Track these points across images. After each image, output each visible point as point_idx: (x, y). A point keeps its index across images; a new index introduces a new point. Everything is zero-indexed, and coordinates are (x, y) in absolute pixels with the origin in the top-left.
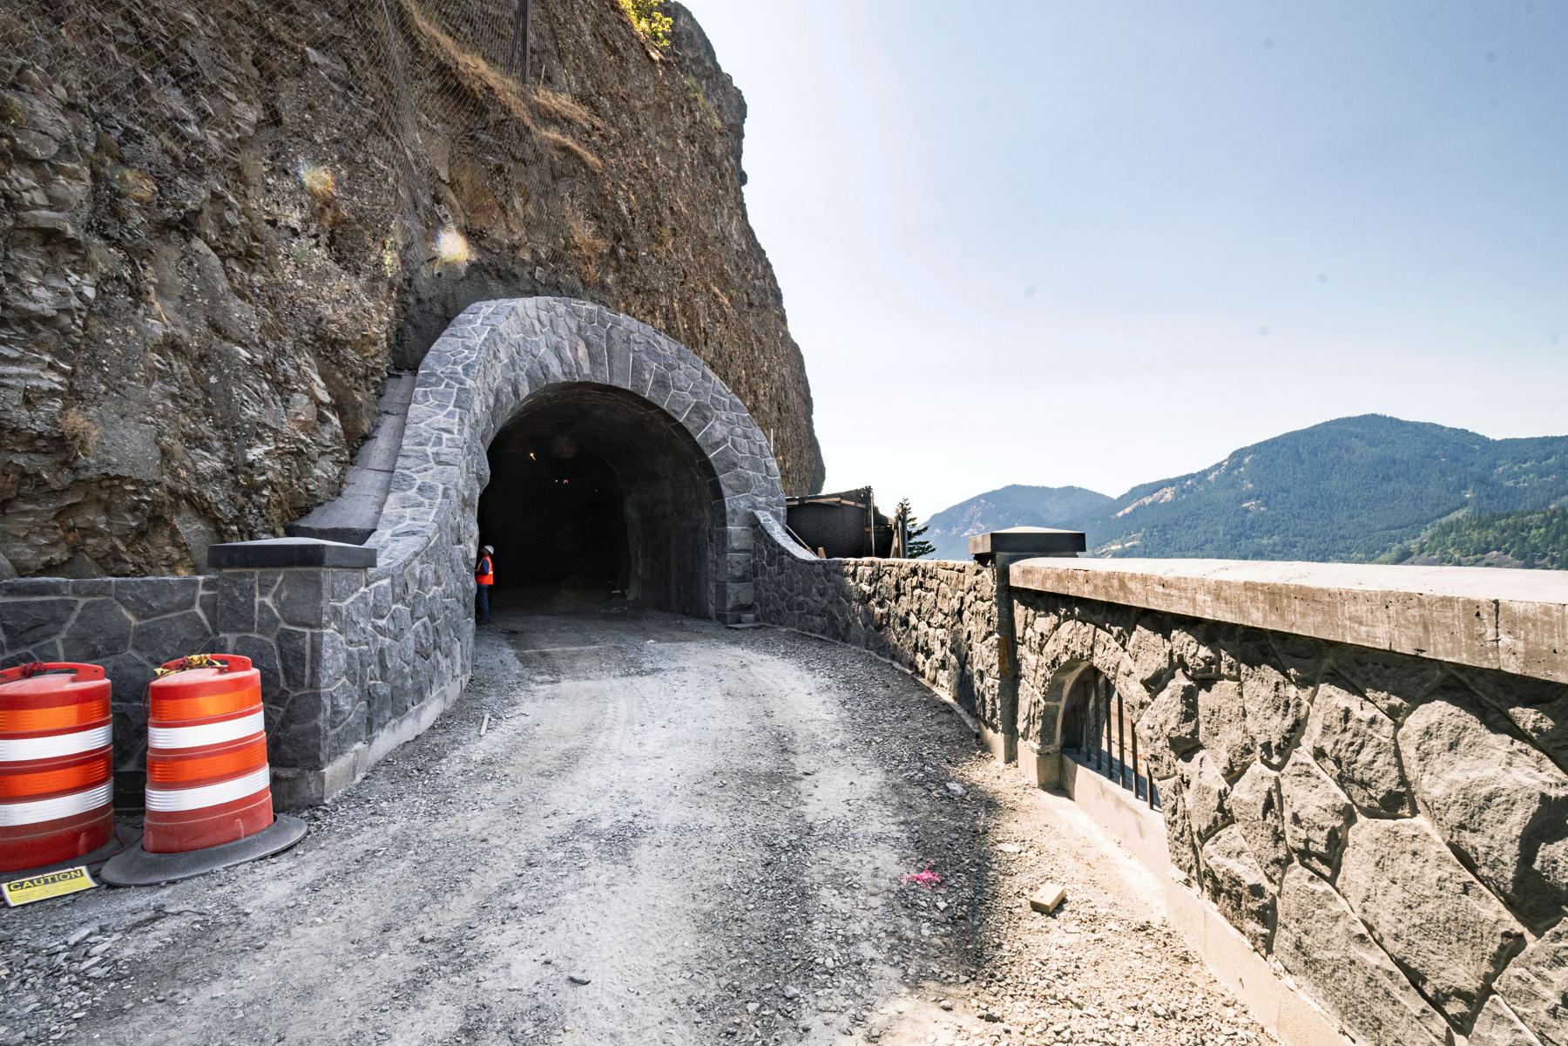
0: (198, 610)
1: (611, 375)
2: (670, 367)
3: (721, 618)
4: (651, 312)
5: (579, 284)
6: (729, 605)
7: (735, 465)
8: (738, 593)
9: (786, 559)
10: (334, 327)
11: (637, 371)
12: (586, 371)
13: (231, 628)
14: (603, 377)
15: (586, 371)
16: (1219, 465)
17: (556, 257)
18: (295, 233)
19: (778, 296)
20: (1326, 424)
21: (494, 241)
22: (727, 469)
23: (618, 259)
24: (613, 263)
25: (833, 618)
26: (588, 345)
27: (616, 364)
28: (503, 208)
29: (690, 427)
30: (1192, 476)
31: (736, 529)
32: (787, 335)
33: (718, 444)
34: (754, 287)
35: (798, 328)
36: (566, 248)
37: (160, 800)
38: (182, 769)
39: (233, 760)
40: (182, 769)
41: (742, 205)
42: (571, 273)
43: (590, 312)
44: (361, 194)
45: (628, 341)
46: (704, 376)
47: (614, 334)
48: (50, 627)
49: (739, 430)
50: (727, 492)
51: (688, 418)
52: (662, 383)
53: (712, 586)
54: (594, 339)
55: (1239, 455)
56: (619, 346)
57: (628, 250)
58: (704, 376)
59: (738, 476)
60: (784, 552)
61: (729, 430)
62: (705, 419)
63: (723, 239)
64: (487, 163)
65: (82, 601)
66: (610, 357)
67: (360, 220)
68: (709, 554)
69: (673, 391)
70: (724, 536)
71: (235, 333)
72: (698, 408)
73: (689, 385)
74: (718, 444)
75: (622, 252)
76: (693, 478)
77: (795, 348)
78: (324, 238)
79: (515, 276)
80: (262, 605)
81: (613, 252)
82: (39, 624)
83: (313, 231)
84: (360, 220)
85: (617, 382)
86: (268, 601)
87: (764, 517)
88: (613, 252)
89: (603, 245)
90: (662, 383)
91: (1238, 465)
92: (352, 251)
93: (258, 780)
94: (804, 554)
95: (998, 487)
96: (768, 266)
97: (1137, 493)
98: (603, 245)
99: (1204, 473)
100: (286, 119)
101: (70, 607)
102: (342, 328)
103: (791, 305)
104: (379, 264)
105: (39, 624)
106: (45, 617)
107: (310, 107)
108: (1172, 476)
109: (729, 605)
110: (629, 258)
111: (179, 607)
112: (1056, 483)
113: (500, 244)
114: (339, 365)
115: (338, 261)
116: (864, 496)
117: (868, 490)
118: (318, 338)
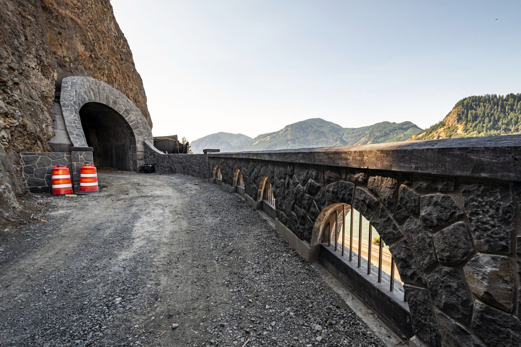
0: (65, 158)
1: (100, 99)
2: (117, 98)
3: (135, 170)
4: (103, 75)
5: (83, 68)
6: (138, 167)
7: (138, 127)
8: (140, 163)
9: (156, 154)
10: (45, 93)
11: (107, 98)
12: (93, 99)
13: (75, 162)
14: (98, 101)
15: (93, 99)
16: (282, 130)
17: (76, 60)
18: (34, 69)
19: (130, 54)
20: (309, 120)
21: (58, 55)
22: (136, 129)
23: (92, 58)
24: (91, 60)
25: (171, 168)
26: (93, 90)
27: (101, 96)
28: (61, 45)
29: (124, 116)
30: (274, 133)
31: (139, 146)
32: (135, 70)
33: (132, 121)
34: (122, 51)
35: (139, 68)
36: (78, 56)
37: (82, 184)
38: (85, 180)
39: (93, 180)
40: (85, 180)
41: (114, 18)
42: (81, 65)
43: (93, 81)
44: (48, 58)
45: (104, 90)
46: (127, 101)
47: (100, 88)
48: (35, 161)
49: (139, 118)
50: (135, 135)
51: (123, 113)
52: (115, 103)
53: (131, 162)
54: (94, 89)
55: (287, 127)
56: (101, 91)
57: (95, 55)
58: (127, 101)
59: (139, 131)
60: (155, 152)
61: (133, 118)
62: (129, 114)
63: (109, 30)
64: (55, 31)
65: (40, 157)
66: (99, 94)
67: (49, 66)
68: (130, 153)
69: (118, 105)
70: (135, 148)
71: (35, 99)
72: (126, 110)
73: (122, 104)
74: (132, 121)
75: (93, 55)
76: (123, 130)
77: (139, 76)
78: (40, 70)
79: (65, 66)
80: (81, 158)
81: (91, 56)
82: (32, 160)
83: (37, 68)
84: (49, 66)
85: (101, 102)
86: (82, 157)
87: (147, 142)
88: (91, 56)
89: (88, 54)
90: (115, 103)
91: (287, 130)
92: (46, 73)
93: (96, 184)
94: (162, 153)
95: (216, 133)
96: (125, 41)
97: (259, 137)
98: (88, 54)
99: (278, 132)
100: (29, 39)
101: (38, 157)
102: (47, 93)
103: (136, 59)
104: (53, 76)
105: (32, 160)
106: (33, 159)
107: (33, 35)
108: (270, 132)
109: (138, 167)
110: (95, 58)
111: (62, 158)
112: (235, 132)
113: (60, 57)
114: (47, 103)
115: (44, 76)
116: (175, 137)
117: (176, 136)
118: (42, 96)
